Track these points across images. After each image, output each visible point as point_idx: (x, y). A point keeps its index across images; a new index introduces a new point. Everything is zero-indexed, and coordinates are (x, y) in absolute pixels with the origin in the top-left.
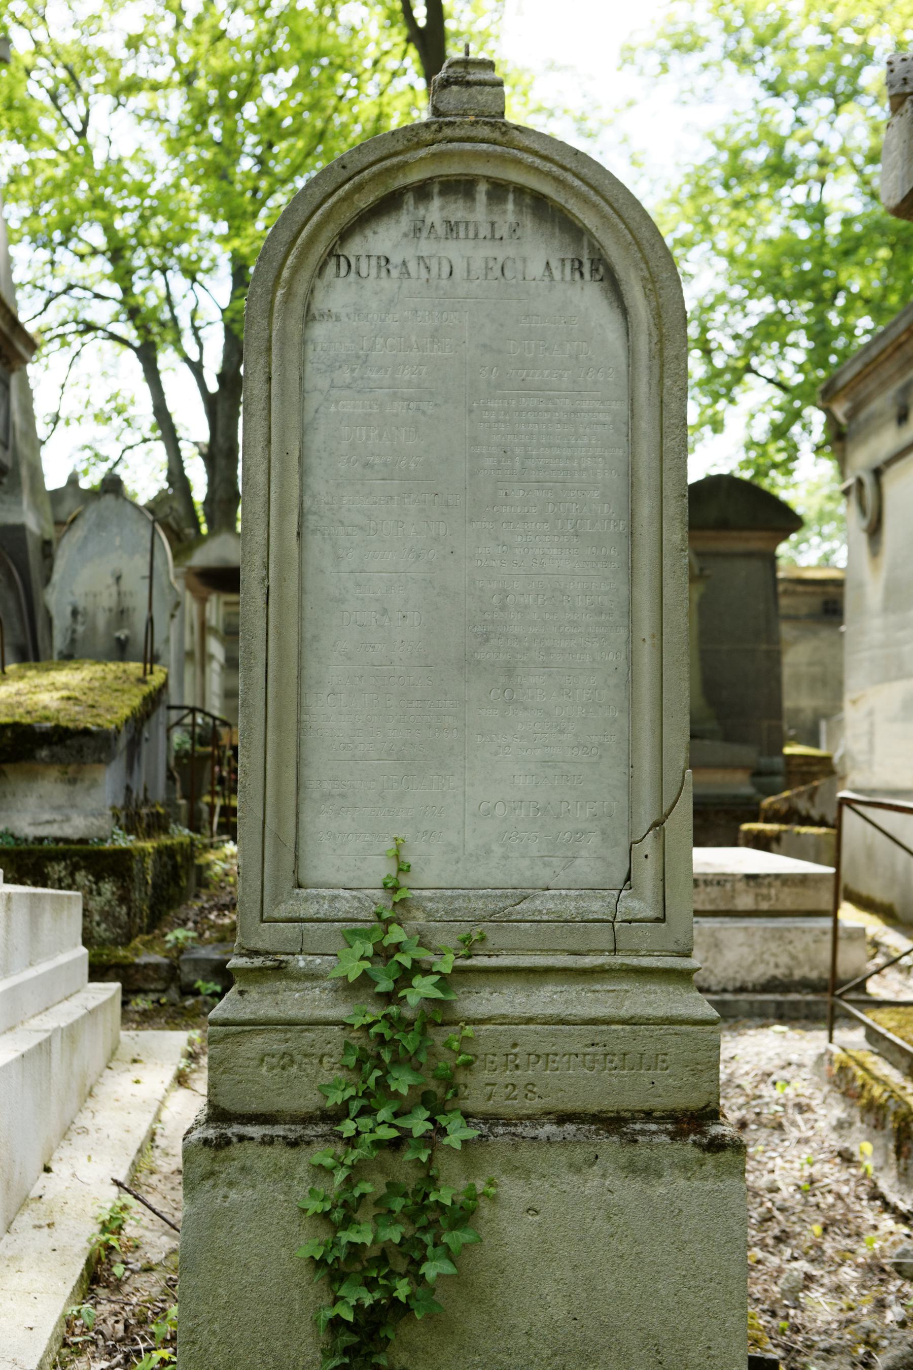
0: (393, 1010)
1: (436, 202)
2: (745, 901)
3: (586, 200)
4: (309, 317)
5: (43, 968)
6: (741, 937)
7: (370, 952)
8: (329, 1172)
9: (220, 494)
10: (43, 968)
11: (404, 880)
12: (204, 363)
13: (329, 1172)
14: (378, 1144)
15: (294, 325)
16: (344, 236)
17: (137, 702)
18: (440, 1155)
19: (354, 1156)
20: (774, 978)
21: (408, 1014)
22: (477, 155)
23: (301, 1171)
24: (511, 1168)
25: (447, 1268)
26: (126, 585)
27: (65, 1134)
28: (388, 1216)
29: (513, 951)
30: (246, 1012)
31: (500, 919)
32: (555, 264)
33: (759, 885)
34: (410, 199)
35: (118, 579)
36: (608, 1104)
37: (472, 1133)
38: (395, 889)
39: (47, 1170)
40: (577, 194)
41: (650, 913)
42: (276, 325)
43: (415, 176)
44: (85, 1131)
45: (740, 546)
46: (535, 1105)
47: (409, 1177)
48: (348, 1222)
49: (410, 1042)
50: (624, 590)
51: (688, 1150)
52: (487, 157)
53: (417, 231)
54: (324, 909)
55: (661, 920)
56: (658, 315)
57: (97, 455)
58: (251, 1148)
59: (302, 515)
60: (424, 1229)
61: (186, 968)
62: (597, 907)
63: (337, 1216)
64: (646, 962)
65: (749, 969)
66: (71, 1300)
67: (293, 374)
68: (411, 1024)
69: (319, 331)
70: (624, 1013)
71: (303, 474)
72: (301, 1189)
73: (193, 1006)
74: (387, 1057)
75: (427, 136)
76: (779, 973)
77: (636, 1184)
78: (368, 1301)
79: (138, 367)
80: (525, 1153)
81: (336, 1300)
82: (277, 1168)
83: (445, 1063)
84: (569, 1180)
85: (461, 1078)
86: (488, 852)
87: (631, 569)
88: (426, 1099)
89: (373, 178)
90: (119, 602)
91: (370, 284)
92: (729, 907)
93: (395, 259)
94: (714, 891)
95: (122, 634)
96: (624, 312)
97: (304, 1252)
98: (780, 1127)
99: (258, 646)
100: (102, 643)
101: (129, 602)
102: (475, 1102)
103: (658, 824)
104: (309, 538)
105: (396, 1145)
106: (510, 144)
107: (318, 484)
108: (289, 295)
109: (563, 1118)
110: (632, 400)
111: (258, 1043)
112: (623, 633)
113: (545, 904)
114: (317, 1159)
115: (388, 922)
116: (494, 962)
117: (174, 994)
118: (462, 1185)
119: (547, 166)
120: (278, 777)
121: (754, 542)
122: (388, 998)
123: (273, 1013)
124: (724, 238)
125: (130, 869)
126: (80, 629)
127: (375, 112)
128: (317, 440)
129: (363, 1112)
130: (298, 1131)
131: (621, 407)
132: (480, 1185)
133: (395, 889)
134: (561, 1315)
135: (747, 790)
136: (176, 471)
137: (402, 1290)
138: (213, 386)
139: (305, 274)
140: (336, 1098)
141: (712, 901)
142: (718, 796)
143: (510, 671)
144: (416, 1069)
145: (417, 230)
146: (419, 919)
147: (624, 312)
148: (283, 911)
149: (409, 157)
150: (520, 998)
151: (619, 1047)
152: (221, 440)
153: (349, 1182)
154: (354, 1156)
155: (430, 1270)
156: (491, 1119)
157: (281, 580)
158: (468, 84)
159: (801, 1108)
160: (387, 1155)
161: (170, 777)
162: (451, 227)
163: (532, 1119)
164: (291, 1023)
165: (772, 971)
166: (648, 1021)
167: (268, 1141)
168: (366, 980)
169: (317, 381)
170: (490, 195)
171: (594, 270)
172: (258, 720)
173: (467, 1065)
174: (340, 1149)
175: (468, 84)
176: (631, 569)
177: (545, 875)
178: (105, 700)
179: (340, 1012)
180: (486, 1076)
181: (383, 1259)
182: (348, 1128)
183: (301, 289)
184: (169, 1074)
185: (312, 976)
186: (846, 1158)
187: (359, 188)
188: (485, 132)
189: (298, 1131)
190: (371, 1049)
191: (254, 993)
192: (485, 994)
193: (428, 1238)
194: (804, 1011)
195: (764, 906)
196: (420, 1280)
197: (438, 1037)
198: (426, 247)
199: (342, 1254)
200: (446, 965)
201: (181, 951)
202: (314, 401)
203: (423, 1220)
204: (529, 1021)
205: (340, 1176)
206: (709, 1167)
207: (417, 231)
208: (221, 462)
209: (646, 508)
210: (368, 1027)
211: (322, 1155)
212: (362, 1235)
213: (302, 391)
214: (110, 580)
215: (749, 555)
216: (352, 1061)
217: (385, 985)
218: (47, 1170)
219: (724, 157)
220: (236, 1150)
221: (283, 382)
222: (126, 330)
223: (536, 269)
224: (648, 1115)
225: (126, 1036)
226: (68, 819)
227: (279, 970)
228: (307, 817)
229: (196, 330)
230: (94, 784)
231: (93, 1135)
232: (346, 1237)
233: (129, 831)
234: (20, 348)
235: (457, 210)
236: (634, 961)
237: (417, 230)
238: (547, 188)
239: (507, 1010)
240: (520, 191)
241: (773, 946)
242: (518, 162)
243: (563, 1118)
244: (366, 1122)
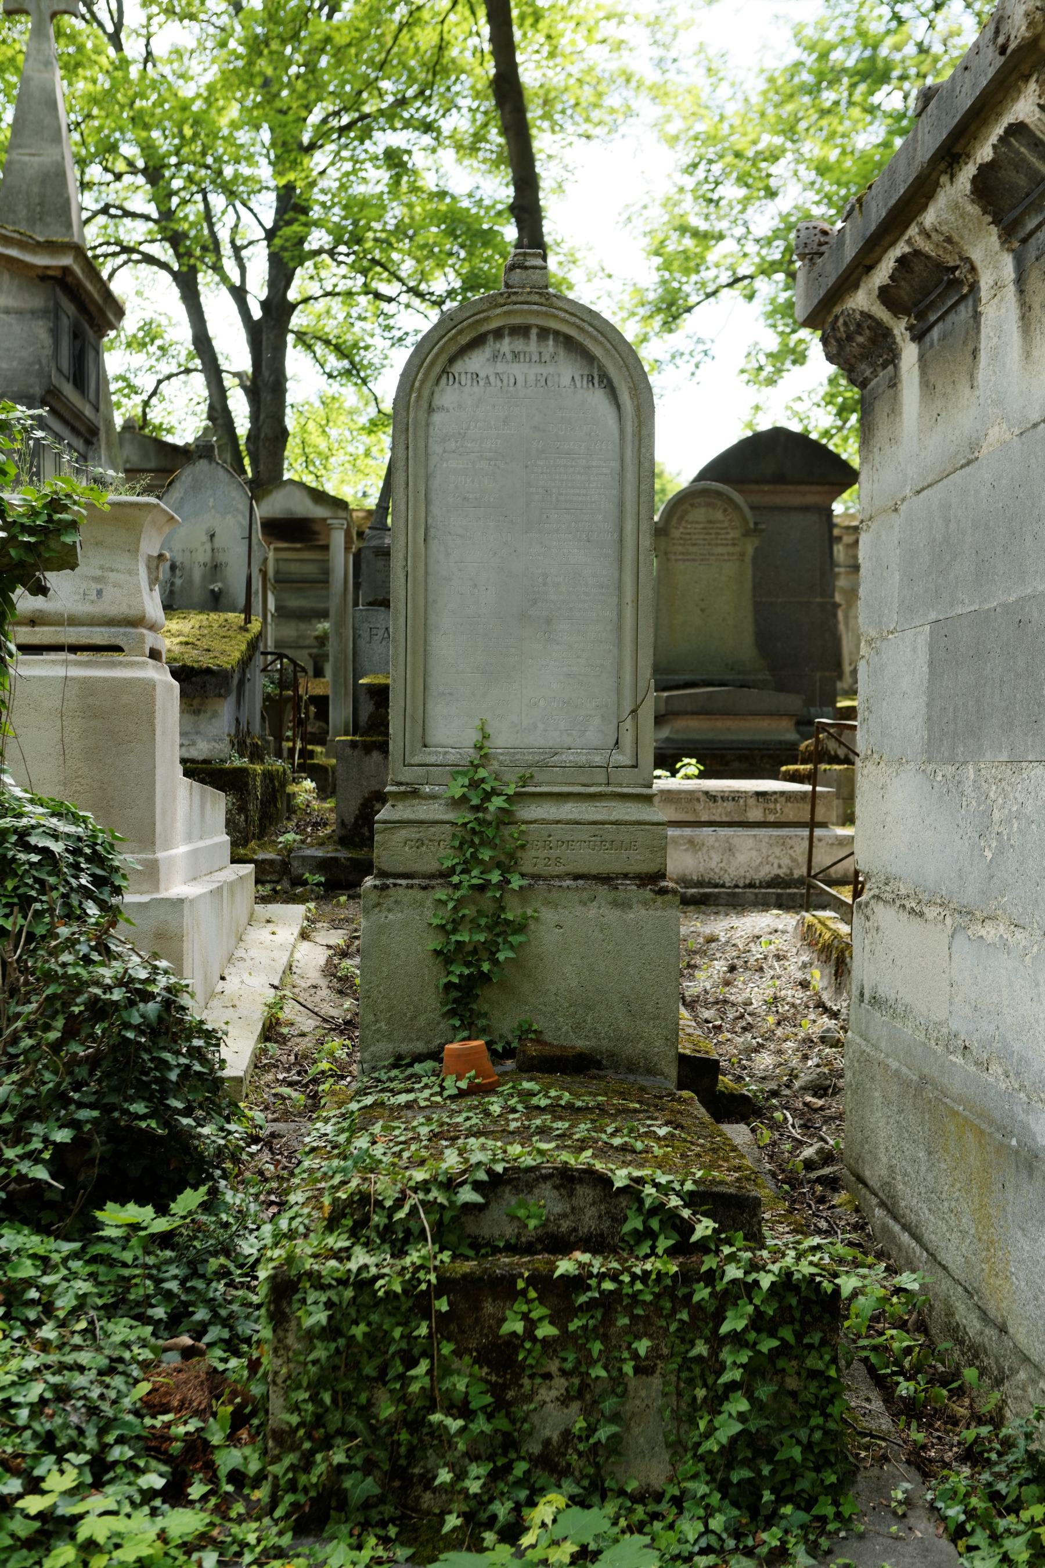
0: (480, 815)
1: (507, 340)
2: (755, 814)
3: (596, 340)
4: (430, 410)
5: (208, 842)
6: (750, 843)
7: (467, 782)
8: (445, 903)
9: (266, 431)
10: (208, 842)
11: (486, 743)
12: (248, 288)
13: (445, 903)
14: (472, 887)
15: (422, 415)
16: (452, 360)
17: (244, 647)
18: (507, 895)
19: (458, 894)
20: (778, 876)
21: (489, 817)
22: (531, 312)
23: (429, 903)
24: (547, 903)
25: (512, 955)
26: (219, 542)
27: (230, 959)
28: (476, 927)
29: (548, 784)
30: (396, 816)
31: (543, 766)
32: (577, 378)
33: (767, 801)
34: (491, 338)
35: (212, 536)
36: (603, 869)
37: (524, 882)
38: (481, 748)
39: (223, 978)
40: (591, 336)
41: (629, 763)
42: (412, 415)
43: (494, 325)
44: (242, 959)
45: (797, 500)
46: (561, 869)
47: (488, 906)
48: (455, 931)
49: (490, 832)
50: (616, 575)
51: (647, 893)
52: (537, 313)
53: (495, 357)
54: (440, 759)
55: (635, 766)
56: (638, 410)
57: (129, 386)
58: (400, 890)
59: (426, 529)
60: (498, 935)
61: (295, 864)
62: (598, 759)
63: (449, 927)
64: (625, 790)
65: (757, 870)
66: (259, 1041)
67: (421, 444)
68: (490, 823)
69: (437, 418)
70: (612, 818)
71: (428, 502)
72: (429, 913)
73: (302, 894)
74: (477, 841)
75: (501, 301)
76: (781, 872)
77: (616, 913)
78: (466, 972)
79: (175, 292)
80: (555, 895)
81: (449, 973)
82: (415, 901)
83: (509, 846)
84: (579, 910)
85: (519, 854)
86: (536, 727)
87: (621, 561)
88: (499, 865)
89: (469, 326)
90: (213, 558)
91: (467, 389)
92: (742, 819)
93: (482, 375)
94: (729, 805)
95: (216, 587)
96: (619, 407)
97: (431, 947)
98: (761, 969)
99: (401, 606)
100: (198, 594)
101: (222, 558)
102: (527, 868)
103: (634, 711)
104: (430, 542)
105: (481, 888)
106: (551, 306)
107: (436, 510)
108: (419, 397)
109: (577, 877)
110: (622, 460)
111: (403, 833)
112: (615, 600)
113: (568, 757)
114: (438, 896)
115: (477, 766)
116: (538, 789)
117: (285, 884)
118: (519, 912)
119: (573, 319)
120: (413, 683)
121: (811, 497)
122: (477, 808)
123: (412, 817)
124: (812, 148)
125: (247, 784)
126: (178, 582)
127: (435, 40)
128: (436, 483)
129: (463, 872)
130: (425, 882)
131: (615, 465)
132: (529, 912)
133: (481, 748)
134: (574, 984)
135: (792, 736)
136: (218, 407)
137: (486, 967)
138: (257, 313)
139: (429, 384)
140: (448, 864)
141: (728, 814)
142: (764, 742)
143: (548, 621)
144: (494, 847)
145: (495, 357)
146: (495, 765)
147: (619, 407)
148: (416, 760)
149: (490, 313)
150: (553, 810)
151: (609, 837)
152: (266, 373)
153: (455, 909)
154: (458, 894)
155: (501, 956)
156: (536, 877)
157: (415, 567)
158: (526, 268)
159: (778, 958)
160: (477, 895)
161: (263, 718)
162: (516, 355)
163: (559, 877)
164: (422, 822)
165: (776, 871)
166: (626, 823)
167: (410, 887)
168: (464, 799)
169: (436, 448)
170: (539, 336)
171: (601, 382)
172: (402, 649)
173: (522, 847)
174: (450, 891)
175: (526, 268)
176: (621, 561)
177: (568, 741)
178: (217, 645)
179: (450, 816)
180: (533, 853)
181: (475, 951)
182: (455, 879)
183: (426, 393)
184: (296, 931)
185: (433, 797)
186: (804, 985)
187: (460, 332)
188: (536, 298)
189: (425, 882)
190: (468, 838)
191: (400, 806)
192: (533, 807)
193: (500, 940)
194: (799, 901)
195: (771, 818)
196: (495, 962)
197: (506, 831)
198: (500, 367)
199: (452, 947)
200: (511, 790)
201: (290, 851)
202: (434, 460)
203: (497, 930)
204: (558, 822)
205: (451, 905)
206: (658, 903)
207: (495, 357)
208: (266, 397)
209: (629, 525)
210: (465, 824)
211: (441, 894)
212: (464, 937)
213: (427, 454)
214: (205, 538)
215: (805, 509)
216: (457, 843)
217: (475, 801)
218: (223, 978)
219: (810, 59)
220: (392, 891)
221: (416, 448)
222: (162, 251)
223: (566, 380)
224: (626, 876)
225: (259, 908)
226: (194, 744)
227: (415, 794)
228: (430, 705)
229: (237, 250)
230: (215, 714)
231: (249, 962)
232: (454, 938)
233: (242, 756)
234: (111, 317)
235: (519, 345)
236: (619, 790)
237: (495, 357)
238: (572, 332)
239: (545, 816)
240: (557, 333)
241: (777, 851)
242: (555, 317)
243: (577, 877)
244: (465, 877)
